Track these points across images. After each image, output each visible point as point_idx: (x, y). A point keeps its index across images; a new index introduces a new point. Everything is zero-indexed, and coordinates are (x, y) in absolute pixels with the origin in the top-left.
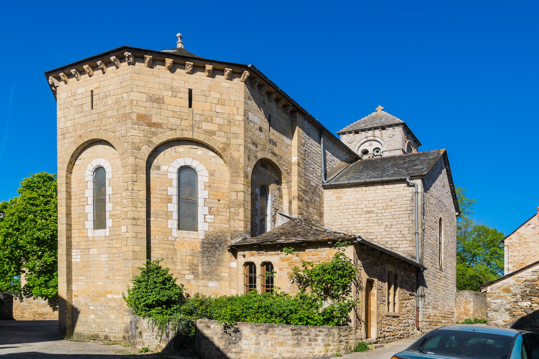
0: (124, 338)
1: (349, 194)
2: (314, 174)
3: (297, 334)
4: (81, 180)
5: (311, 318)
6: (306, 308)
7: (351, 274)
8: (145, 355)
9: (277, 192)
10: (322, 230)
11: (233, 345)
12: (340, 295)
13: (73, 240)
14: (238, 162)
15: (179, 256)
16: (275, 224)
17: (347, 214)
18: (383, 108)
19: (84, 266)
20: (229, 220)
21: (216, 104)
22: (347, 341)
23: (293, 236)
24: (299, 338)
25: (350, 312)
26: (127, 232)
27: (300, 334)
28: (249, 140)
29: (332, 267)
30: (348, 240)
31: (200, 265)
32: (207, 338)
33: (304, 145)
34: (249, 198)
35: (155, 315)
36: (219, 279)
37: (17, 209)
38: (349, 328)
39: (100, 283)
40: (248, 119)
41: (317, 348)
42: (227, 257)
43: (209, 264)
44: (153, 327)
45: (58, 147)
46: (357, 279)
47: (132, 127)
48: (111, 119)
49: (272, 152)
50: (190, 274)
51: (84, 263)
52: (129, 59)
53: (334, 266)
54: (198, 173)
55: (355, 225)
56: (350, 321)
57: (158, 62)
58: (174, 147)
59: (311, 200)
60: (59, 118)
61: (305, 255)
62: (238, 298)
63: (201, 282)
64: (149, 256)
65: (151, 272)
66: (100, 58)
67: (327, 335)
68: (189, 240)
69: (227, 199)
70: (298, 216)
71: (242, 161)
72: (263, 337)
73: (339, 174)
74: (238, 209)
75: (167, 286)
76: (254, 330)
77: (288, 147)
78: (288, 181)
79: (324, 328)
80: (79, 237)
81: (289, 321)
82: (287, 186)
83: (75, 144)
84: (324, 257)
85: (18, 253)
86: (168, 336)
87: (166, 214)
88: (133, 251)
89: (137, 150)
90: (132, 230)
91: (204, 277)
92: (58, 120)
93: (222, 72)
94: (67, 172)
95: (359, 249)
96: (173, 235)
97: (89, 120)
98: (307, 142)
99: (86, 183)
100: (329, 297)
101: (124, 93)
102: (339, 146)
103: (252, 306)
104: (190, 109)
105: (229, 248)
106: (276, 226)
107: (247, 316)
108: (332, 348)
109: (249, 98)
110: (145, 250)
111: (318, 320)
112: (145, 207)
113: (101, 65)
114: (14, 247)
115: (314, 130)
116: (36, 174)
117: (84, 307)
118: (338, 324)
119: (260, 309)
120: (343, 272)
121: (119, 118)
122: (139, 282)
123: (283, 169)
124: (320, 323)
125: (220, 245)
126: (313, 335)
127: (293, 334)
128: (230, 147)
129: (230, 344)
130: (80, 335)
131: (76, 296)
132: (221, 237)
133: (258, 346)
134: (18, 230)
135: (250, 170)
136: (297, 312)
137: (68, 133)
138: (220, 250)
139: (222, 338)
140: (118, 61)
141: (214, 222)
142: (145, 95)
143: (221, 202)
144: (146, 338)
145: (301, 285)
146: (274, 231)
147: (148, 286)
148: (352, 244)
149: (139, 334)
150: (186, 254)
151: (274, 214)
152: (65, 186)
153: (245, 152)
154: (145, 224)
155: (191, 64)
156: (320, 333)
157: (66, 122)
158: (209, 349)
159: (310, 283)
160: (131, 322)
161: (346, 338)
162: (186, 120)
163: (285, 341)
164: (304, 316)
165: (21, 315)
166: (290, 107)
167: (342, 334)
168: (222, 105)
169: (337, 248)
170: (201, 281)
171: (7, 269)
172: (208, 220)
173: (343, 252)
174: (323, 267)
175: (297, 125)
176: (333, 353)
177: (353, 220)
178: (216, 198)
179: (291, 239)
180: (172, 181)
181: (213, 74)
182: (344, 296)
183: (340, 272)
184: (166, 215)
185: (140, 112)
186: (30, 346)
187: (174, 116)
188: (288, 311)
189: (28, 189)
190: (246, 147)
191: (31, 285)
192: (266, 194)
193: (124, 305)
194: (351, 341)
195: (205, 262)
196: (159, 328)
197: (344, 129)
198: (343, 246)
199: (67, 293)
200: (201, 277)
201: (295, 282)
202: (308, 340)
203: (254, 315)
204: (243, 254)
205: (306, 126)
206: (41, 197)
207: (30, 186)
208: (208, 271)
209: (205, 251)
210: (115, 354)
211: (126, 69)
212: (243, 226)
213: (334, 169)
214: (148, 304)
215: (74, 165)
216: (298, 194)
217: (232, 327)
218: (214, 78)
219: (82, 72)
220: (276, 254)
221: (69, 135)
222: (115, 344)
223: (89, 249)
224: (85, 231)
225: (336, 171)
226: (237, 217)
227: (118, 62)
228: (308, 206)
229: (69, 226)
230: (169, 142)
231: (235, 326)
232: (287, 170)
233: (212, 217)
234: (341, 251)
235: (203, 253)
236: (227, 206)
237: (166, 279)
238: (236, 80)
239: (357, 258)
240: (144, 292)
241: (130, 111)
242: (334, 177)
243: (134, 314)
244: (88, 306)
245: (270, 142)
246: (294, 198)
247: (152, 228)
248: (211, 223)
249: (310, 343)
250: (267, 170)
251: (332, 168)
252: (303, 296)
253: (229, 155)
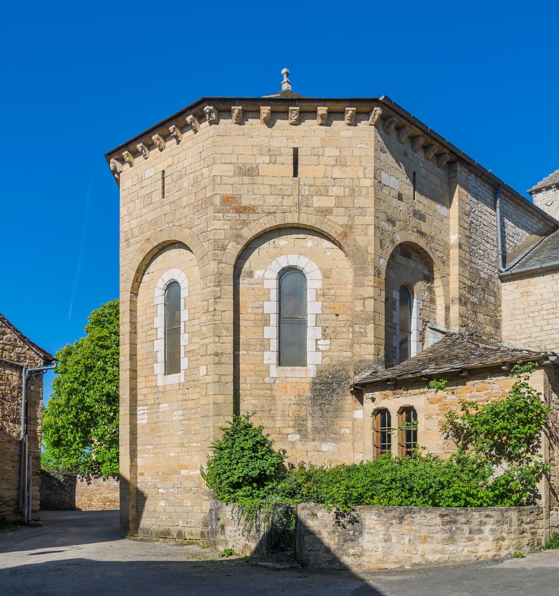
0: (202, 534)
1: (542, 285)
2: (486, 260)
3: (450, 522)
4: (150, 303)
5: (473, 496)
6: (466, 478)
7: (539, 418)
8: (226, 561)
9: (427, 293)
10: (495, 348)
11: (350, 544)
12: (522, 453)
13: (139, 392)
14: (365, 253)
15: (280, 407)
16: (423, 345)
17: (539, 318)
19: (152, 430)
20: (352, 346)
21: (333, 166)
22: (534, 530)
23: (447, 362)
24: (454, 529)
25: (539, 482)
26: (207, 375)
27: (455, 522)
28: (382, 216)
29: (508, 408)
30: (534, 362)
31: (310, 418)
32: (312, 533)
33: (468, 215)
34: (382, 308)
35: (242, 499)
36: (337, 438)
37: (83, 355)
38: (537, 510)
39: (172, 454)
40: (380, 182)
41: (482, 544)
42: (349, 403)
43: (322, 416)
44: (239, 517)
45: (121, 259)
46: (550, 425)
47: (215, 217)
48: (187, 209)
49: (418, 231)
50: (295, 433)
51: (153, 425)
52: (210, 115)
53: (511, 407)
54: (307, 276)
55: (553, 336)
56: (540, 497)
57: (250, 114)
58: (273, 240)
59: (480, 302)
60: (122, 218)
61: (467, 391)
62: (362, 467)
63: (311, 445)
64: (236, 410)
65: (237, 434)
66: (173, 121)
67: (500, 521)
68: (294, 380)
69: (349, 313)
70: (460, 330)
71: (371, 249)
72: (395, 529)
73: (526, 255)
74: (364, 326)
75: (259, 453)
76: (382, 518)
77: (444, 220)
78: (443, 275)
79: (495, 510)
80: (146, 387)
81: (437, 501)
82: (443, 283)
83: (142, 251)
84: (496, 393)
85: (84, 416)
86: (258, 531)
87: (261, 343)
88: (214, 404)
89: (220, 251)
90: (214, 371)
91: (315, 437)
92: (121, 219)
93: (341, 114)
94: (132, 294)
95: (553, 374)
96: (271, 375)
97: (159, 214)
98: (474, 209)
99: (155, 307)
100: (505, 459)
102: (526, 210)
103: (380, 478)
104: (295, 178)
105: (352, 389)
106: (425, 347)
107: (373, 495)
108: (508, 543)
109: (381, 150)
110: (232, 401)
111: (485, 497)
112: (232, 335)
113: (174, 131)
114: (79, 409)
115: (485, 189)
116: (107, 304)
117: (152, 490)
118: (518, 503)
119: (394, 483)
120: (527, 415)
121: (198, 205)
122: (221, 449)
123: (435, 256)
124: (487, 502)
125: (339, 384)
126: (476, 523)
127: (443, 522)
128: (353, 230)
129: (345, 541)
130: (147, 531)
131: (142, 474)
132: (341, 372)
133: (388, 543)
134: (83, 383)
135: (383, 263)
136: (450, 486)
137: (133, 237)
138: (339, 393)
139: (334, 532)
140: (196, 121)
141: (330, 350)
142: (232, 166)
143: (340, 318)
144: (230, 534)
145: (460, 440)
146: (420, 356)
147: (232, 456)
148: (541, 366)
149: (220, 529)
150: (289, 402)
151: (421, 330)
152: (129, 315)
153: (375, 236)
154: (232, 362)
155: (295, 110)
156: (488, 519)
157: (132, 222)
158: (315, 550)
159: (473, 437)
160: (211, 511)
161: (531, 525)
162: (290, 197)
163: (431, 535)
164: (461, 491)
165: (89, 502)
166: (447, 155)
167: (524, 520)
168: (341, 167)
169: (516, 376)
170: (310, 443)
171: (72, 439)
172: (321, 348)
173: (526, 382)
174: (493, 409)
175: (457, 183)
176: (509, 552)
177: (550, 327)
178: (333, 312)
179: (443, 366)
180: (269, 292)
181: (328, 119)
182: (529, 455)
183: (521, 415)
184: (260, 345)
185: (225, 193)
186: (80, 549)
187: (273, 193)
188: (437, 485)
189: (97, 326)
190: (377, 227)
191: (100, 461)
192: (410, 299)
193: (202, 486)
194: (540, 531)
195: (318, 412)
196: (247, 519)
197: (539, 184)
198: (526, 371)
199: (131, 471)
200: (311, 437)
201: (450, 437)
202: (468, 531)
203: (384, 494)
204: (371, 396)
205: (473, 184)
206: (112, 335)
207: (100, 321)
208: (321, 426)
209: (317, 396)
210: (187, 560)
211: (206, 132)
212: (373, 352)
213: (519, 247)
214: (232, 482)
215: (141, 282)
216: (460, 294)
217: (347, 515)
218: (330, 125)
219: (151, 146)
220: (421, 393)
221: (134, 239)
222: (190, 544)
223: (159, 404)
224: (154, 378)
225: (520, 252)
226: (363, 340)
227: (196, 123)
228: (475, 313)
229: (133, 371)
230: (266, 232)
231: (353, 513)
232: (442, 257)
233: (328, 342)
234: (522, 379)
235: (314, 399)
236: (349, 322)
237: (258, 442)
238: (363, 124)
239: (551, 390)
240: (226, 464)
241: (212, 194)
242: (518, 260)
243: (215, 498)
244: (156, 489)
245: (414, 215)
246: (453, 301)
247: (242, 367)
248: (325, 351)
249: (471, 536)
250: (411, 261)
251: (515, 246)
252: (462, 459)
253: (352, 243)
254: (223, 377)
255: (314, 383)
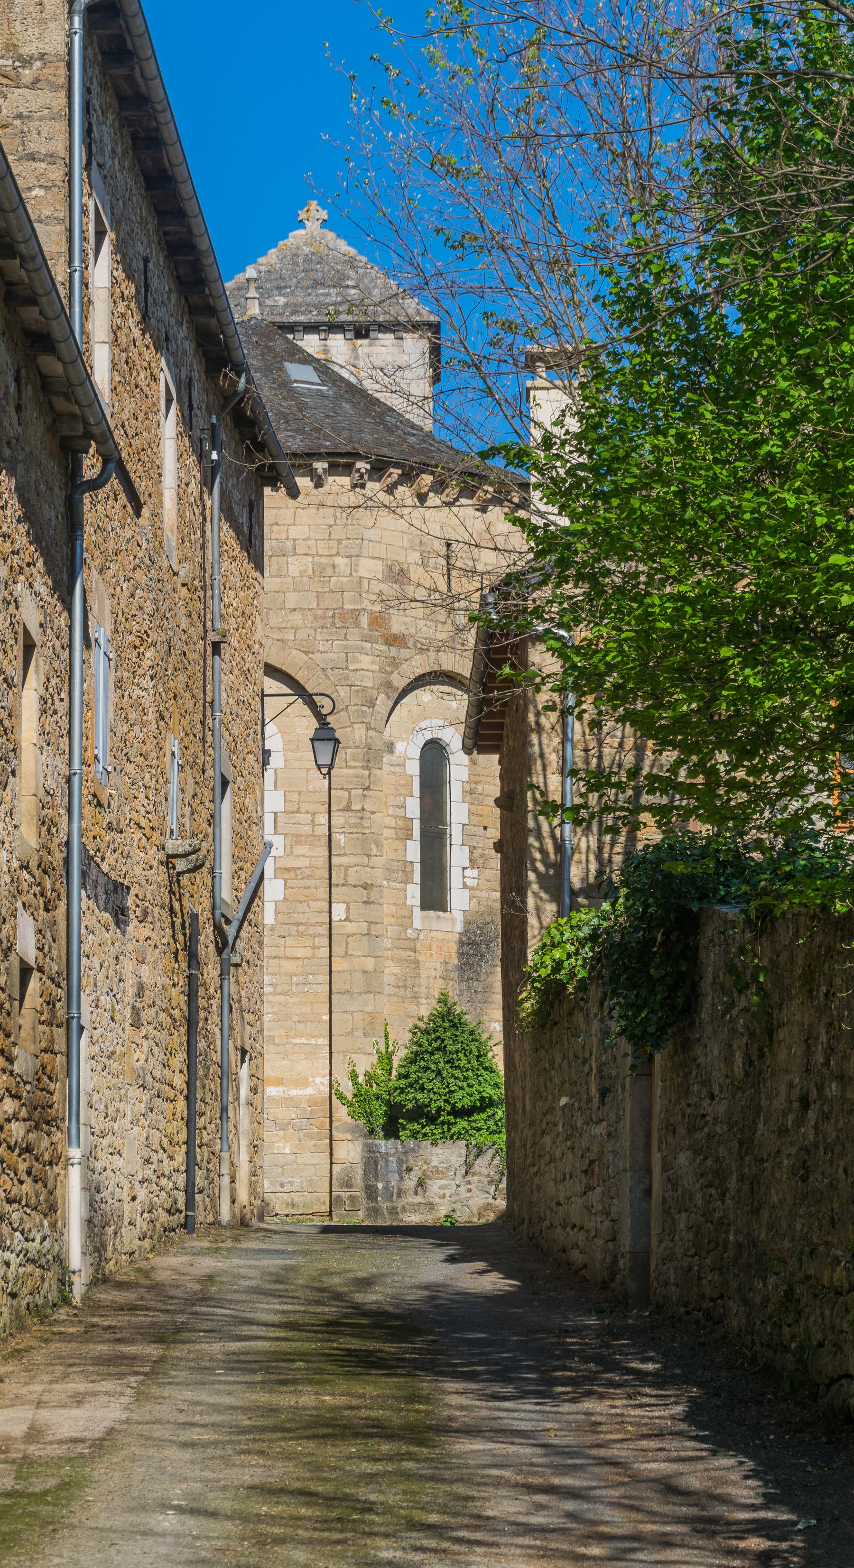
18: (324, 215)
68: (439, 935)
101: (338, 554)
121: (324, 617)
142: (380, 563)
172: (469, 882)
235: (461, 969)
254: (373, 927)
255: (461, 943)
